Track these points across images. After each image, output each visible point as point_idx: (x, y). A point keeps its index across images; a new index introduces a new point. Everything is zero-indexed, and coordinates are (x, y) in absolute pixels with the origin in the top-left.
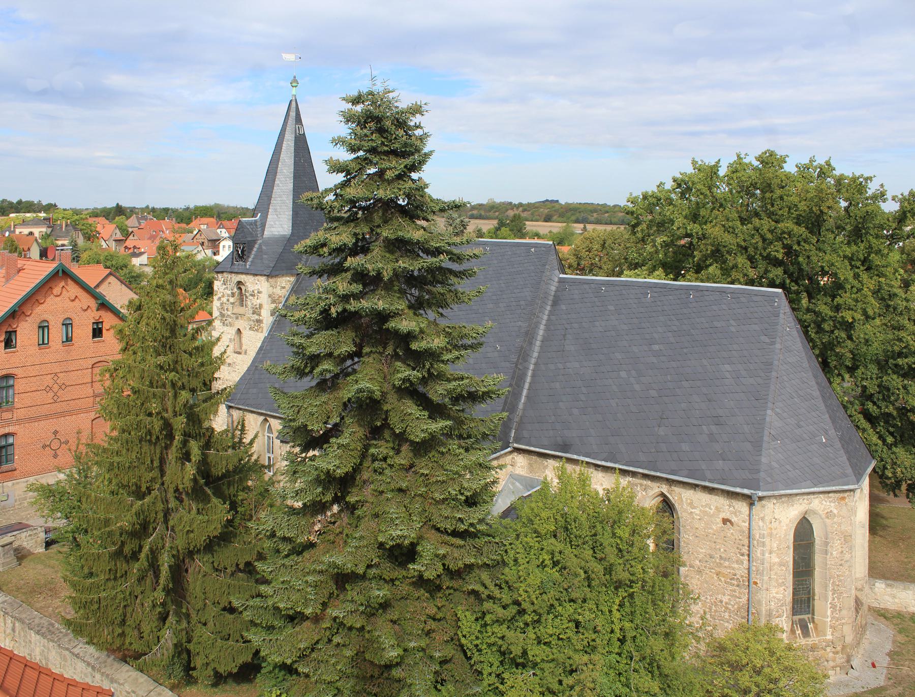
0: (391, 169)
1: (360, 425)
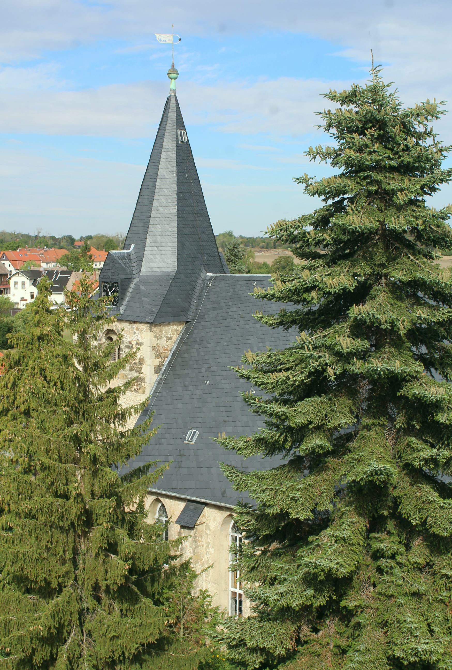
0: (402, 190)
1: (360, 515)
